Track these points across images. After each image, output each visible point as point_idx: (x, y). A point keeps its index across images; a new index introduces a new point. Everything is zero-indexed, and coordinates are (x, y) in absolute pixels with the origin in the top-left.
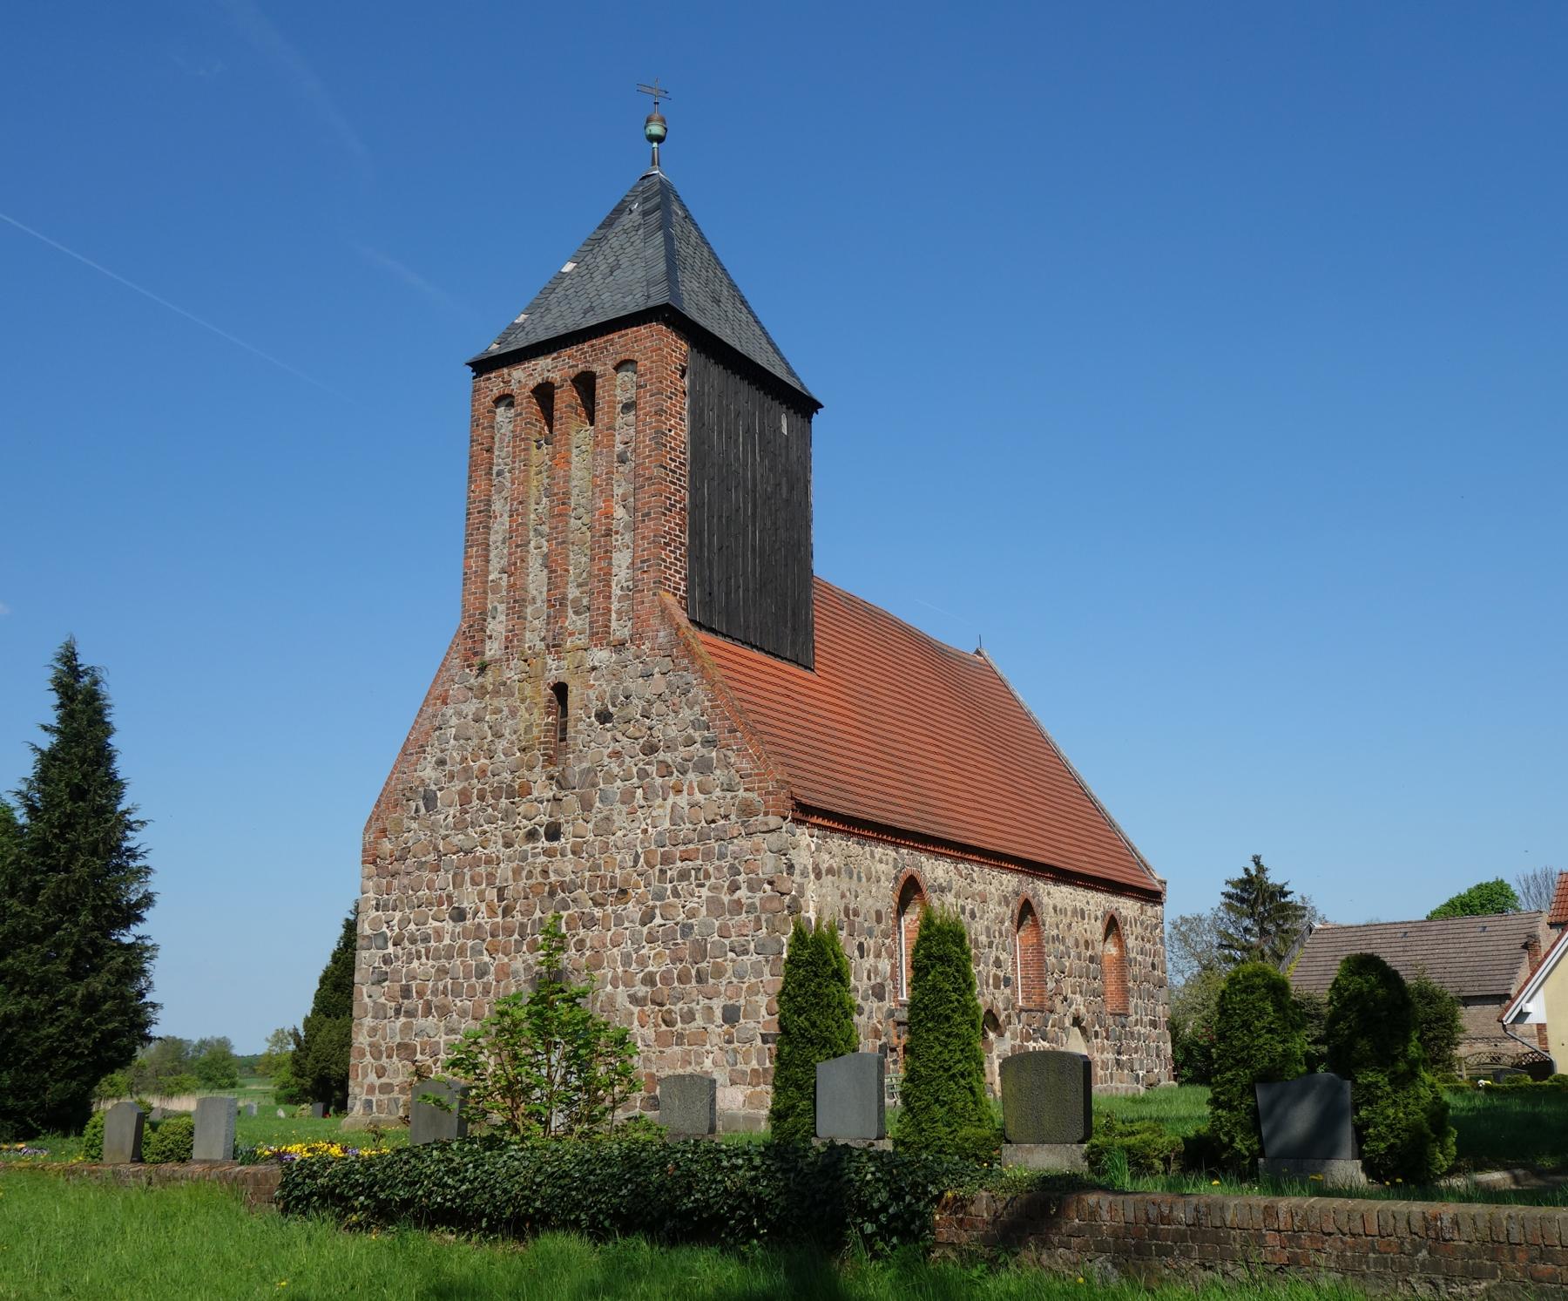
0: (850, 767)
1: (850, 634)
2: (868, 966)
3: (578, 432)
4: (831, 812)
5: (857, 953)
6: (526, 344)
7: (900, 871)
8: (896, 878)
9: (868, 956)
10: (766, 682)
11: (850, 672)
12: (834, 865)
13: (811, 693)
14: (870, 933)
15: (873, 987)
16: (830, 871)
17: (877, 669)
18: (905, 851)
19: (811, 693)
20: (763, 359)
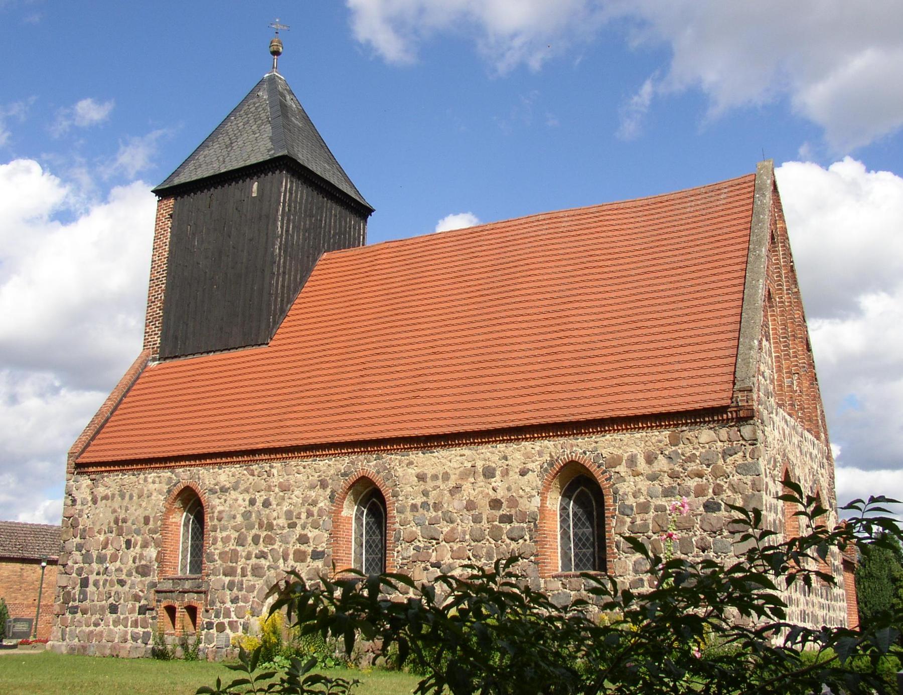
0: (159, 415)
1: (223, 392)
2: (134, 554)
3: (139, 515)
4: (126, 460)
5: (124, 546)
6: (262, 160)
7: (175, 485)
8: (169, 491)
9: (134, 547)
10: (136, 429)
11: (218, 431)
12: (109, 493)
13: (167, 406)
14: (138, 532)
15: (137, 568)
16: (106, 498)
17: (228, 430)
18: (181, 470)
19: (167, 406)
20: (318, 167)
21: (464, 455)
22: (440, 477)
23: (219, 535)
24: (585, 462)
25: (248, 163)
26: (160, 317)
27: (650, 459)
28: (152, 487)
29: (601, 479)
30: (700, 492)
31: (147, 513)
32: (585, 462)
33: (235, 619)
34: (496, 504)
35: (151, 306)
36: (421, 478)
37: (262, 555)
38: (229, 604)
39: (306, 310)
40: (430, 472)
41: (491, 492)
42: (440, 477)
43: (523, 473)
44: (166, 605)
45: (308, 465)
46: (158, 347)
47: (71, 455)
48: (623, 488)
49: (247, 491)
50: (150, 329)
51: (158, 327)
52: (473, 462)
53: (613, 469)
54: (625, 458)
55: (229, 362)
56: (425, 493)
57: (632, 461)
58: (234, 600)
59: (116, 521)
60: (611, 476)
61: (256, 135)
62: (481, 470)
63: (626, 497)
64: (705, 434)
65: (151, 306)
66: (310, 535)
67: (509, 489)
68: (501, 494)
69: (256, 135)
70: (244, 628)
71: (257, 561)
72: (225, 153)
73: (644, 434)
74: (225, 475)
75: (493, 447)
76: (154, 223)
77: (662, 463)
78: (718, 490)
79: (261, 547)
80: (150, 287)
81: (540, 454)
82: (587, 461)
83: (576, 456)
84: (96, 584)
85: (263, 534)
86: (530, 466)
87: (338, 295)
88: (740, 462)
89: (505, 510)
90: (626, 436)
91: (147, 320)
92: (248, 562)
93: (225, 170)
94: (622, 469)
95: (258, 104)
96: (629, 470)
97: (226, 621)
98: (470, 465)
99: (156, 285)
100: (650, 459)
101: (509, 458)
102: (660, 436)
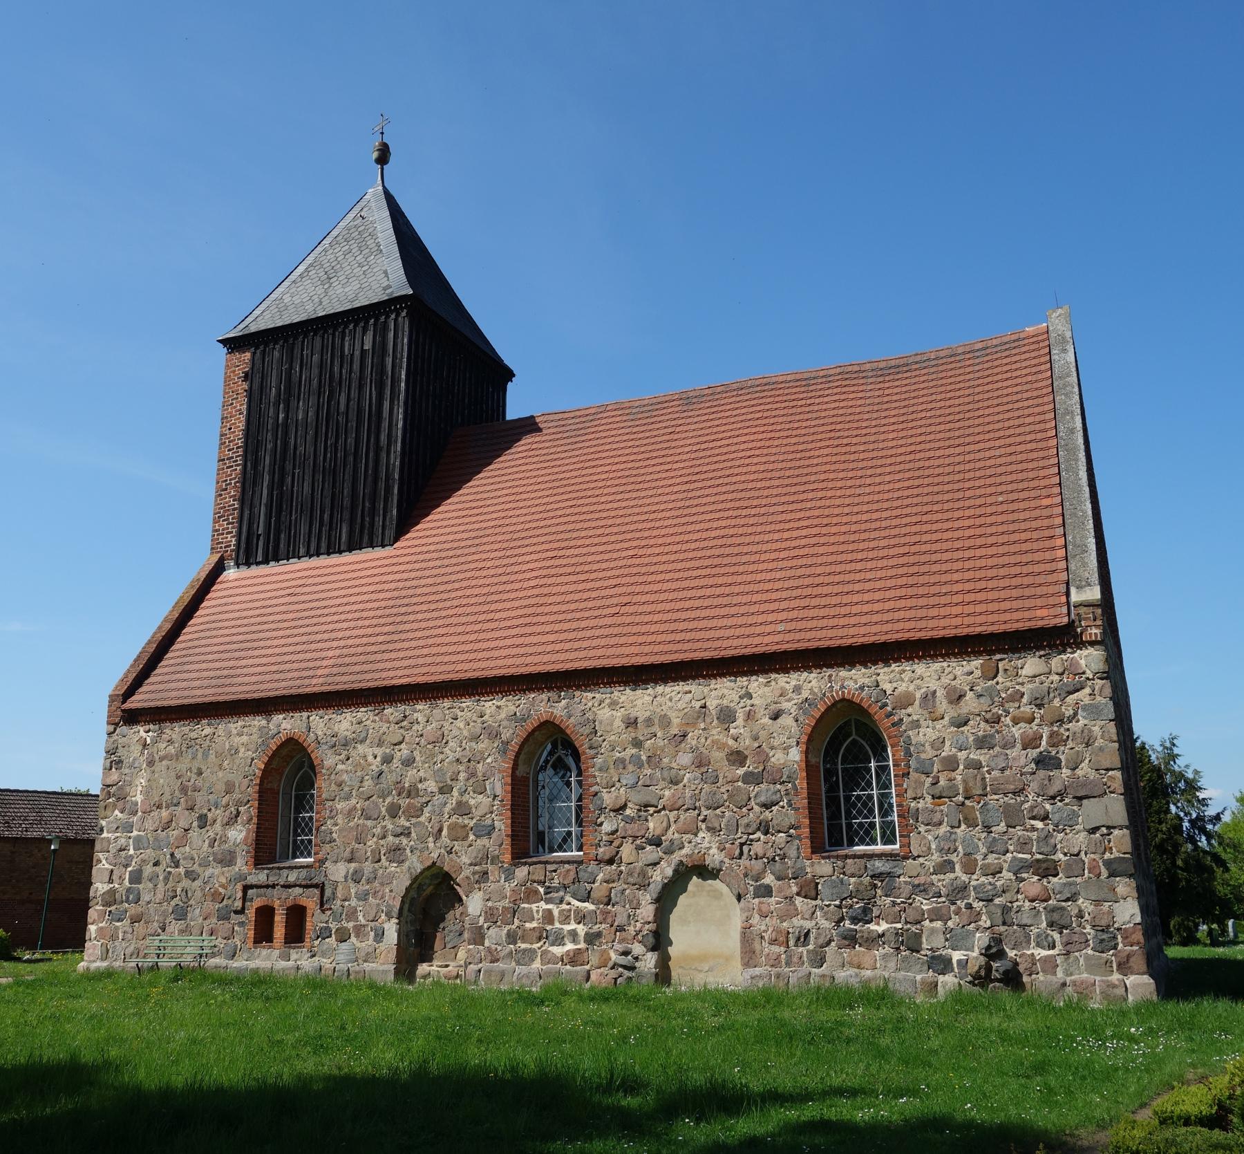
21: (690, 692)
22: (656, 721)
23: (340, 806)
24: (862, 700)
25: (357, 304)
26: (234, 510)
27: (957, 698)
28: (237, 740)
29: (884, 725)
30: (1030, 742)
31: (231, 777)
32: (862, 700)
33: (363, 922)
34: (738, 758)
35: (221, 495)
36: (632, 723)
37: (406, 833)
38: (354, 902)
39: (875, 454)
40: (642, 716)
41: (731, 742)
42: (656, 721)
43: (775, 717)
44: (259, 905)
45: (468, 707)
46: (231, 551)
47: (112, 698)
48: (917, 737)
49: (380, 744)
50: (219, 526)
51: (233, 523)
52: (703, 701)
53: (903, 711)
54: (918, 695)
55: (367, 565)
56: (637, 744)
57: (929, 697)
58: (363, 897)
59: (184, 790)
60: (901, 720)
61: (364, 269)
62: (714, 712)
63: (922, 748)
64: (1031, 664)
65: (221, 495)
66: (472, 802)
67: (756, 738)
68: (746, 743)
69: (364, 269)
70: (376, 935)
71: (397, 841)
72: (320, 290)
73: (945, 664)
74: (345, 722)
75: (731, 681)
76: (222, 384)
77: (970, 703)
78: (1056, 740)
79: (403, 822)
80: (218, 470)
81: (797, 689)
82: (866, 698)
83: (849, 693)
84: (153, 878)
85: (404, 802)
86: (786, 705)
87: (618, 467)
88: (1087, 700)
89: (750, 766)
90: (920, 668)
91: (215, 514)
92: (382, 842)
93: (324, 313)
94: (915, 711)
95: (363, 228)
96: (925, 712)
97: (351, 925)
98: (698, 704)
99: (228, 468)
100: (957, 698)
101: (754, 695)
102: (965, 670)
